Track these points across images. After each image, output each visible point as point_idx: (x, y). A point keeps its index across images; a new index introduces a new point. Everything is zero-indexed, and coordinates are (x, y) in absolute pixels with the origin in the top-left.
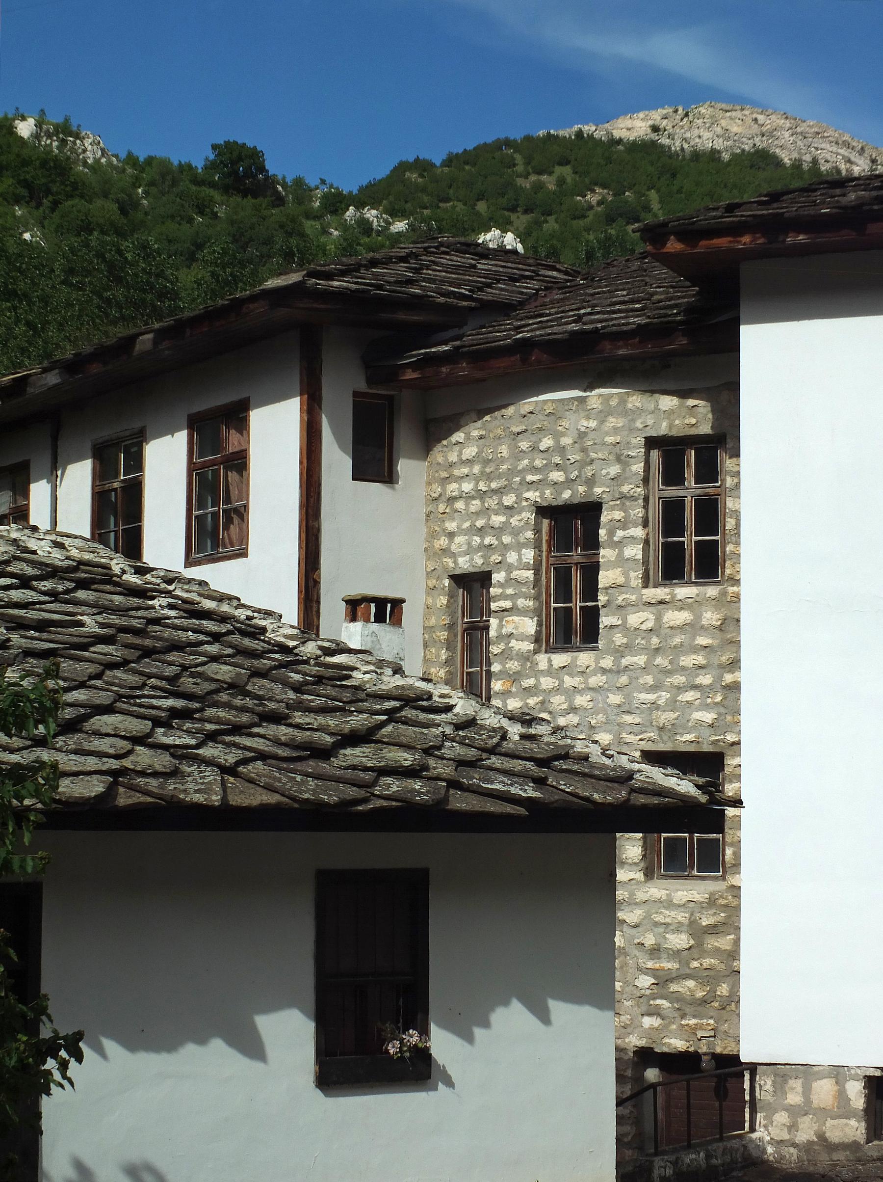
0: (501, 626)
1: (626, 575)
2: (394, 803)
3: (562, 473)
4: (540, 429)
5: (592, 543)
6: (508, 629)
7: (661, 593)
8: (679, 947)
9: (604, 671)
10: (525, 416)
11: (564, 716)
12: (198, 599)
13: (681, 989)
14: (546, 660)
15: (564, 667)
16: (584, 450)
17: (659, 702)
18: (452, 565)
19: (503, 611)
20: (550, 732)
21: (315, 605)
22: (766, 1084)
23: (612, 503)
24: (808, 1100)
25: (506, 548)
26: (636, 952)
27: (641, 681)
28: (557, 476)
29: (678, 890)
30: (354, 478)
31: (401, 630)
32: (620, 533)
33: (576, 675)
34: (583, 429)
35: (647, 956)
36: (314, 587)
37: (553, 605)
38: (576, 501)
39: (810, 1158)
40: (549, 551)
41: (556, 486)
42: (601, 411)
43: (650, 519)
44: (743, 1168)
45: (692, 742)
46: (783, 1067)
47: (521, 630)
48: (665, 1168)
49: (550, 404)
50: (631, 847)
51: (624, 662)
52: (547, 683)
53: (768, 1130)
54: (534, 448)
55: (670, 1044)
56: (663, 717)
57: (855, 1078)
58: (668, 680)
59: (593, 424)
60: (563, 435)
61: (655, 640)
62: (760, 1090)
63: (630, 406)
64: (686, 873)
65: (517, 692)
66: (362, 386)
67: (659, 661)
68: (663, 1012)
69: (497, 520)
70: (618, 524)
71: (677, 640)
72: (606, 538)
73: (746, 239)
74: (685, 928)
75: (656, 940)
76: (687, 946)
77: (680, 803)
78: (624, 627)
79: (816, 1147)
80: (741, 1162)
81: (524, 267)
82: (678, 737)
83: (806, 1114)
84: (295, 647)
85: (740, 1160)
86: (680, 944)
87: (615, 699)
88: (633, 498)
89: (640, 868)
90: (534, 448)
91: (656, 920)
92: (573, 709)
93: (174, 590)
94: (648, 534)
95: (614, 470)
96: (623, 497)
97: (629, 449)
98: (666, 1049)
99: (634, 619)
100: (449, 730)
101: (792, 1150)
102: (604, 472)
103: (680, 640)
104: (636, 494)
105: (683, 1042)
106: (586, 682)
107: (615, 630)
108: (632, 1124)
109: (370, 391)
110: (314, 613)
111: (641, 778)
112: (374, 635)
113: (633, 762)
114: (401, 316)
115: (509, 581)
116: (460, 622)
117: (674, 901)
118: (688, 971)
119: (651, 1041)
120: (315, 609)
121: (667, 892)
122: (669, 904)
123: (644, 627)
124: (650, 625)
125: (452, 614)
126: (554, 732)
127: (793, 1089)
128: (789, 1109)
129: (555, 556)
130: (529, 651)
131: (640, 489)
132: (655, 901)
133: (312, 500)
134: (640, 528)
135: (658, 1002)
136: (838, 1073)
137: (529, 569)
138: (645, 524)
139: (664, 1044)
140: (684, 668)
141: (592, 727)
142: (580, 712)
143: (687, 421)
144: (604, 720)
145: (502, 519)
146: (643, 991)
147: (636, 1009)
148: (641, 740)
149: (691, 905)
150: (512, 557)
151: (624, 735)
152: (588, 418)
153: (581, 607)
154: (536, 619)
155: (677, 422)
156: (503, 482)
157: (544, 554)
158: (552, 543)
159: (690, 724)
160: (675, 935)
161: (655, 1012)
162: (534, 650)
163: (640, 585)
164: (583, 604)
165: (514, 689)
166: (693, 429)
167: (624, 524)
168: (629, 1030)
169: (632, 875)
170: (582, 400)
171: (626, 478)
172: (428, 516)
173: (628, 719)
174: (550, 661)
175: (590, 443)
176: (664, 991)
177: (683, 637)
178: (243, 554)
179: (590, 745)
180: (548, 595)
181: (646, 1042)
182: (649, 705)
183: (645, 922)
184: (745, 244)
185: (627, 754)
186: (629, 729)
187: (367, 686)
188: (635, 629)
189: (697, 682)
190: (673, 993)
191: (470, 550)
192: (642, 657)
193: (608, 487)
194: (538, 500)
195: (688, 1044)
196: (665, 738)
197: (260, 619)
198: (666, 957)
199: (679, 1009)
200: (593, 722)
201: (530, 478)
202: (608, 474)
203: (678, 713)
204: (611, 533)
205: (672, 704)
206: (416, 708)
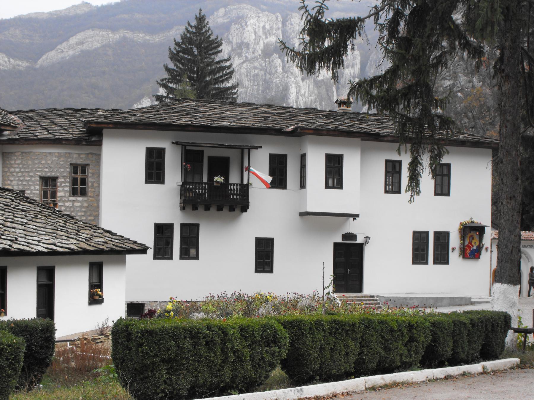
1: (65, 193)
5: (55, 185)
25: (30, 185)
32: (63, 184)
69: (28, 179)
71: (78, 209)
78: (64, 206)
81: (228, 121)
90: (40, 163)
124: (71, 205)
156: (30, 170)
178: (327, 187)
191: (18, 185)
201: (38, 170)
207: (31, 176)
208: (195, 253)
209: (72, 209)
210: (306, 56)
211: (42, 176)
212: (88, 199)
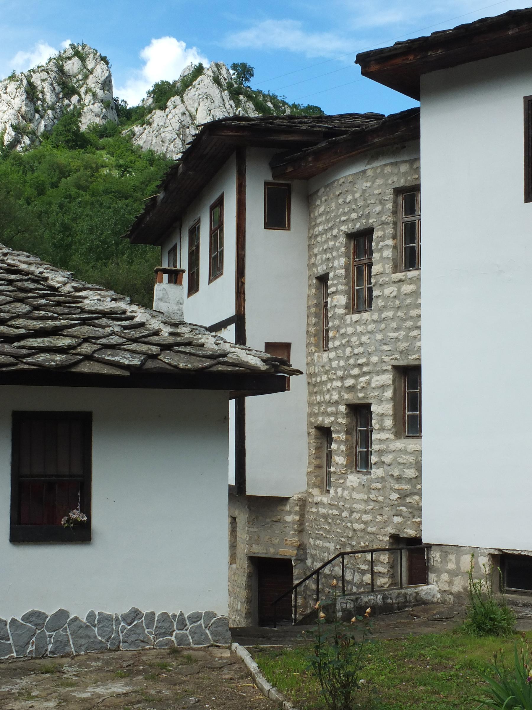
0: (332, 301)
1: (384, 267)
2: (33, 367)
3: (355, 214)
4: (347, 191)
6: (335, 303)
7: (399, 276)
8: (410, 477)
9: (374, 322)
10: (341, 185)
11: (357, 348)
12: (18, 264)
13: (412, 501)
14: (350, 318)
15: (357, 321)
16: (365, 200)
17: (400, 338)
18: (316, 272)
19: (333, 293)
20: (189, 331)
21: (242, 295)
22: (436, 555)
23: (378, 227)
24: (458, 568)
26: (390, 480)
27: (391, 326)
28: (354, 216)
29: (410, 444)
30: (265, 228)
31: (181, 287)
32: (381, 244)
33: (362, 325)
34: (364, 188)
35: (395, 482)
36: (242, 285)
37: (356, 288)
38: (362, 228)
39: (460, 602)
40: (354, 258)
41: (354, 221)
42: (373, 177)
43: (398, 234)
44: (415, 606)
45: (416, 359)
46: (445, 547)
47: (340, 303)
48: (346, 603)
49: (350, 176)
50: (387, 420)
51: (383, 316)
52: (350, 330)
53: (437, 584)
54: (345, 202)
55: (407, 533)
56: (401, 346)
57: (483, 555)
58: (404, 324)
59: (369, 184)
60: (356, 192)
61: (397, 302)
62: (433, 560)
63: (386, 171)
64: (418, 435)
65: (339, 337)
66: (270, 178)
67: (399, 314)
68: (404, 514)
70: (380, 239)
71: (408, 301)
72: (375, 247)
73: (411, 57)
74: (413, 466)
75: (399, 472)
76: (414, 477)
77: (249, 371)
79: (462, 595)
80: (413, 602)
82: (410, 357)
83: (457, 575)
84: (59, 287)
85: (413, 601)
86: (411, 475)
87: (379, 337)
88: (387, 224)
89: (391, 432)
91: (399, 461)
92: (361, 344)
93: (6, 260)
94: (396, 243)
95: (378, 208)
96: (383, 223)
97: (385, 196)
98: (405, 536)
99: (387, 291)
100: (117, 329)
101: (450, 596)
102: (374, 210)
103: (409, 301)
104: (389, 221)
105: (413, 532)
106: (366, 329)
107: (379, 298)
108: (389, 578)
109: (275, 181)
110: (242, 300)
111: (233, 357)
112: (164, 290)
113: (232, 347)
114: (283, 137)
115: (336, 276)
116: (322, 302)
117: (408, 451)
118: (416, 491)
119: (397, 531)
120: (242, 297)
121: (405, 445)
122: (405, 452)
123: (392, 295)
125: (317, 299)
126: (192, 331)
127: (451, 560)
128: (449, 572)
129: (356, 261)
130: (343, 314)
131: (391, 218)
132: (398, 451)
133: (240, 240)
134: (391, 240)
135: (401, 508)
136: (474, 552)
137: (342, 269)
138: (394, 237)
139: (404, 533)
140: (412, 317)
141: (369, 354)
142: (364, 346)
143: (414, 177)
144: (374, 349)
145: (333, 243)
146: (393, 502)
147: (390, 512)
148: (392, 359)
149: (416, 453)
150: (336, 263)
151: (383, 357)
152: (367, 181)
153: (368, 288)
154: (346, 296)
155: (409, 178)
157: (352, 260)
158: (355, 253)
159: (415, 349)
160: (409, 470)
161: (399, 514)
162: (345, 313)
163: (391, 272)
164: (368, 286)
165: (337, 336)
166: (417, 181)
167: (382, 238)
168: (387, 524)
169: (388, 436)
170: (364, 172)
171: (384, 213)
172: (308, 247)
173: (386, 348)
174: (351, 318)
175: (367, 195)
176: (404, 502)
177: (411, 300)
179: (209, 338)
180: (353, 282)
181: (395, 531)
182: (395, 339)
183: (394, 462)
184: (411, 60)
185: (229, 343)
186: (386, 353)
187: (86, 307)
188: (388, 297)
189: (418, 325)
190: (408, 503)
192: (391, 312)
193: (376, 218)
194: (346, 230)
195: (416, 533)
196: (403, 358)
197: (47, 273)
198: (404, 482)
199: (411, 513)
200: (370, 351)
202: (375, 211)
203: (409, 343)
204: (377, 245)
205: (407, 337)
206: (108, 318)
211: (349, 232)
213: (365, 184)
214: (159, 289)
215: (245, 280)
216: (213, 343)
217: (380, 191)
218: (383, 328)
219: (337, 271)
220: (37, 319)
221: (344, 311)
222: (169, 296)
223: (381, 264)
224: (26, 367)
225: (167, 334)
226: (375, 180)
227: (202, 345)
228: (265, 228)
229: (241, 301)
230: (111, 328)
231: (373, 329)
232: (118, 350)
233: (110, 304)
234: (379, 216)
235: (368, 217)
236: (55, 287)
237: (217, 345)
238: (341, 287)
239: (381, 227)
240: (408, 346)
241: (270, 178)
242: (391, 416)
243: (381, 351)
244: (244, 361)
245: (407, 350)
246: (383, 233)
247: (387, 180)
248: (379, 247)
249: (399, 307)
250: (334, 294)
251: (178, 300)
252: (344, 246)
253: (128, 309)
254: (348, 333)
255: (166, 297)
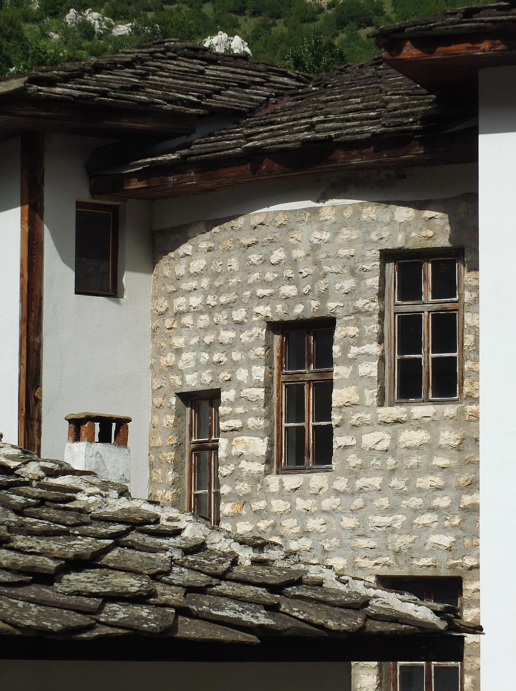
2: (120, 631)
3: (294, 287)
4: (271, 241)
9: (338, 493)
10: (255, 228)
11: (296, 540)
15: (296, 489)
16: (317, 263)
17: (395, 526)
20: (282, 557)
21: (36, 424)
23: (346, 318)
25: (236, 365)
28: (289, 290)
30: (77, 293)
31: (126, 451)
32: (354, 350)
34: (316, 241)
42: (335, 223)
45: (429, 566)
47: (251, 450)
51: (359, 483)
54: (265, 261)
56: (399, 541)
58: (404, 502)
59: (326, 236)
60: (295, 247)
61: (391, 461)
63: (364, 217)
66: (86, 197)
67: (394, 482)
69: (227, 336)
71: (414, 461)
72: (340, 354)
73: (485, 45)
77: (418, 630)
78: (358, 448)
82: (415, 562)
84: (17, 468)
87: (349, 522)
88: (368, 313)
92: (306, 533)
94: (383, 351)
95: (348, 284)
96: (358, 312)
97: (363, 262)
100: (177, 555)
102: (338, 286)
103: (416, 461)
104: (371, 309)
106: (319, 504)
107: (350, 451)
110: (35, 432)
111: (377, 604)
113: (368, 587)
114: (126, 124)
120: (36, 428)
123: (379, 447)
124: (385, 445)
126: (286, 557)
130: (259, 472)
131: (375, 304)
133: (33, 314)
134: (375, 344)
137: (259, 387)
138: (381, 340)
140: (420, 490)
142: (313, 536)
143: (424, 234)
144: (337, 544)
145: (231, 334)
148: (376, 564)
150: (242, 375)
151: (358, 559)
152: (321, 230)
154: (266, 439)
155: (413, 234)
156: (232, 296)
157: (276, 371)
158: (284, 360)
159: (427, 548)
162: (265, 471)
167: (358, 340)
170: (315, 211)
171: (360, 293)
173: (363, 542)
174: (281, 482)
177: (420, 458)
179: (324, 570)
180: (280, 414)
182: (384, 528)
184: (484, 50)
185: (362, 580)
186: (363, 553)
188: (370, 449)
189: (434, 505)
191: (198, 367)
192: (378, 478)
193: (342, 301)
194: (269, 315)
200: (327, 546)
201: (260, 292)
202: (341, 288)
203: (414, 537)
204: (345, 350)
207: (238, 323)
208: (221, 507)
209: (391, 461)
210: (114, 424)
211: (276, 319)
212: (462, 412)
213: (318, 235)
214: (91, 453)
215: (41, 392)
216: (334, 579)
217: (352, 252)
218: (359, 506)
219: (244, 390)
220: (40, 536)
221: (262, 468)
222: (108, 468)
223: (354, 387)
224: (110, 631)
225: (248, 563)
226: (339, 228)
227: (320, 584)
228: (77, 293)
229: (33, 435)
230: (168, 554)
231: (335, 507)
232: (210, 595)
233: (118, 502)
234: (348, 297)
235: (324, 296)
236: (9, 467)
237: (345, 584)
238: (256, 422)
239: (353, 317)
240: (413, 542)
241: (86, 197)
242: (375, 668)
243: (353, 549)
244: (402, 613)
245: (409, 548)
246: (357, 330)
247: (368, 233)
248: (350, 356)
249: (393, 471)
250: (235, 433)
251: (121, 473)
252: (264, 343)
253: (159, 513)
254: (275, 510)
255: (102, 468)
